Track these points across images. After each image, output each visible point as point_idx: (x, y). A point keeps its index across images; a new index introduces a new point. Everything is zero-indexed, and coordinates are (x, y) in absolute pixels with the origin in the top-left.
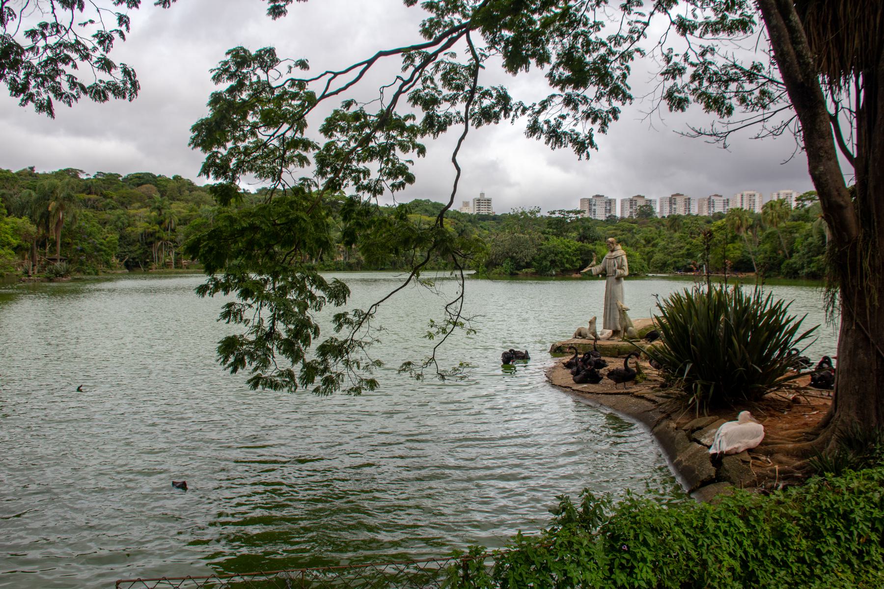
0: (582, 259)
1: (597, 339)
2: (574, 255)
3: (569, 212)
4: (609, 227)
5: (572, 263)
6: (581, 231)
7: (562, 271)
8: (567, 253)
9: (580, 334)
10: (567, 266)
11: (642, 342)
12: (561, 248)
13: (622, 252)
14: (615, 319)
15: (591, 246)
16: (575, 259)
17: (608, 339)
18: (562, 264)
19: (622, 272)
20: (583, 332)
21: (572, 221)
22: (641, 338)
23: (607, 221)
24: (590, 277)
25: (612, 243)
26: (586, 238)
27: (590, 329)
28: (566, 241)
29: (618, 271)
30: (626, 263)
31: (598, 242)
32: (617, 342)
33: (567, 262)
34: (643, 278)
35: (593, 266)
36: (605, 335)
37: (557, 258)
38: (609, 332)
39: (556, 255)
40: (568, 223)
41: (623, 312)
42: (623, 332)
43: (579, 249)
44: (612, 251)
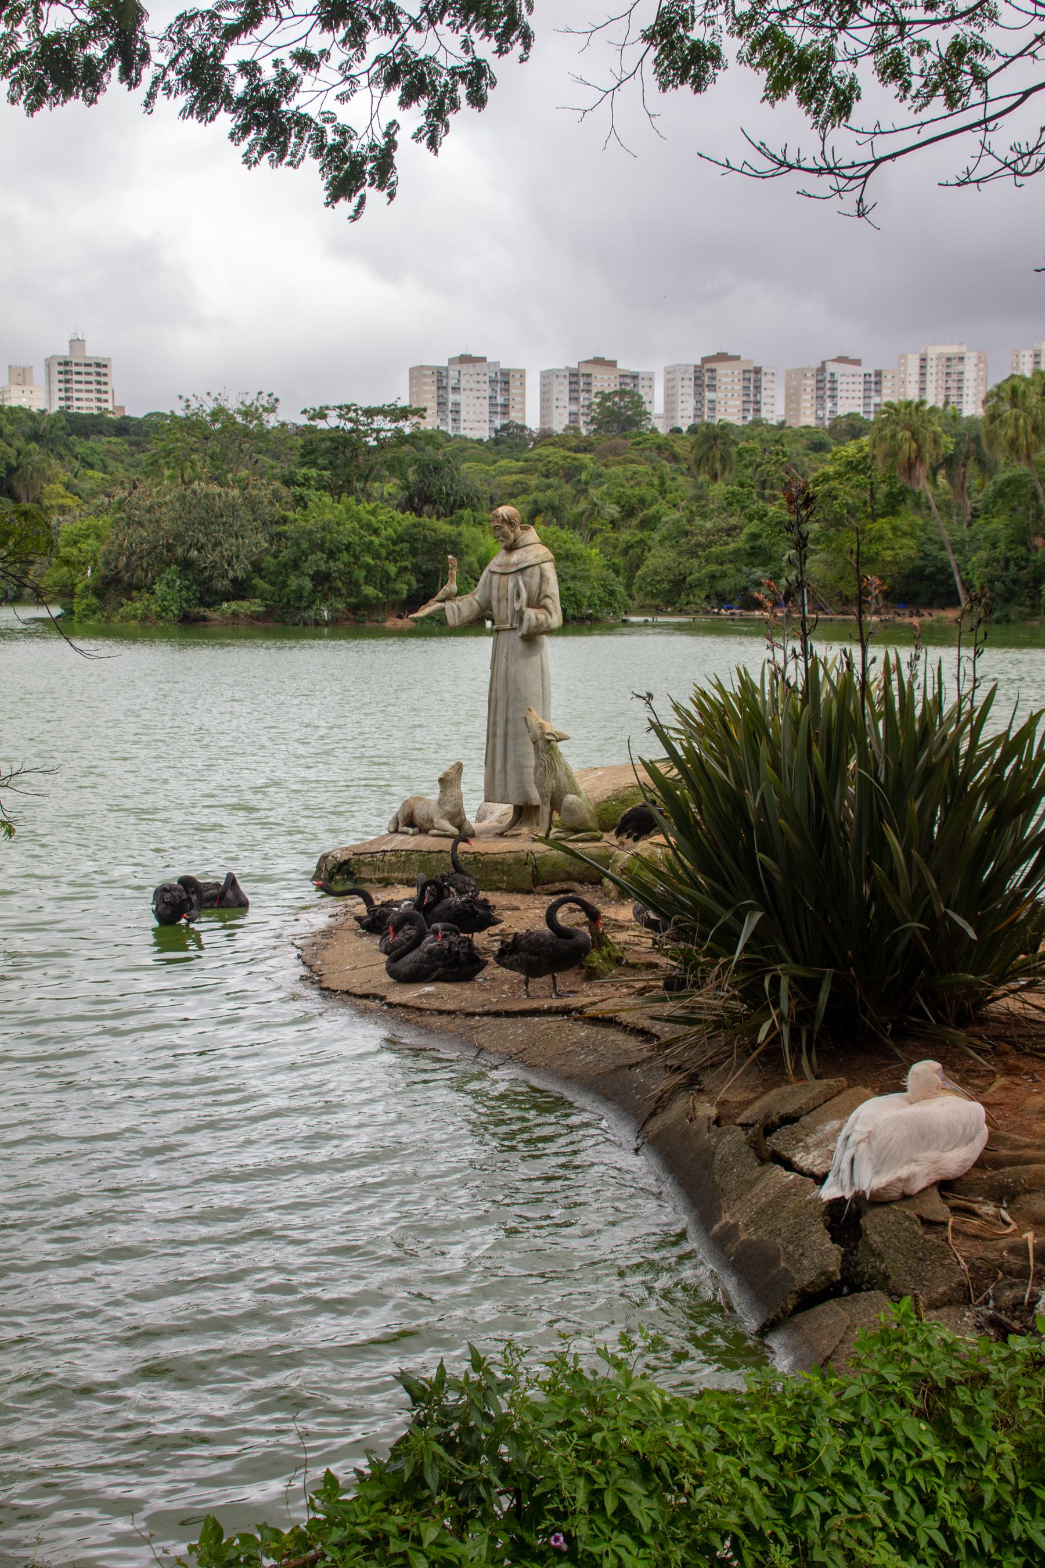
0: (416, 569)
1: (465, 835)
2: (392, 556)
3: (370, 413)
4: (504, 463)
5: (385, 582)
6: (412, 476)
7: (354, 609)
8: (369, 548)
9: (410, 821)
10: (369, 591)
11: (610, 837)
12: (347, 533)
13: (543, 551)
14: (520, 768)
15: (444, 527)
16: (392, 569)
17: (501, 835)
18: (353, 586)
19: (542, 616)
20: (420, 813)
21: (382, 444)
22: (606, 829)
23: (497, 442)
24: (438, 627)
25: (510, 522)
26: (428, 499)
27: (441, 802)
28: (363, 509)
29: (531, 614)
30: (553, 588)
31: (466, 513)
32: (525, 843)
33: (368, 580)
34: (609, 629)
35: (448, 598)
36: (488, 823)
37: (336, 566)
38: (502, 811)
39: (332, 555)
40: (370, 451)
41: (546, 745)
42: (546, 809)
43: (407, 537)
44: (511, 548)
